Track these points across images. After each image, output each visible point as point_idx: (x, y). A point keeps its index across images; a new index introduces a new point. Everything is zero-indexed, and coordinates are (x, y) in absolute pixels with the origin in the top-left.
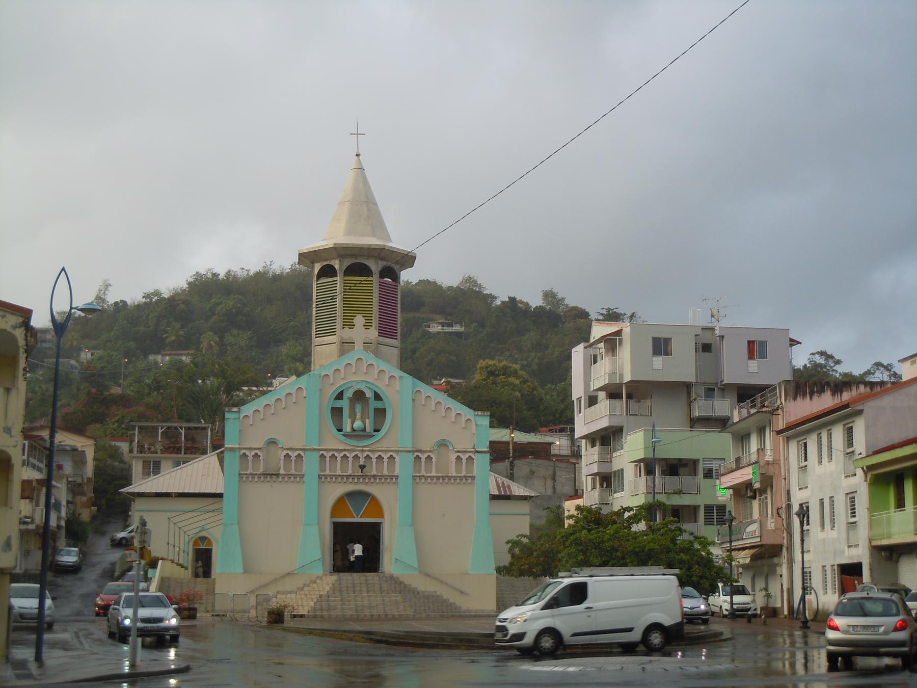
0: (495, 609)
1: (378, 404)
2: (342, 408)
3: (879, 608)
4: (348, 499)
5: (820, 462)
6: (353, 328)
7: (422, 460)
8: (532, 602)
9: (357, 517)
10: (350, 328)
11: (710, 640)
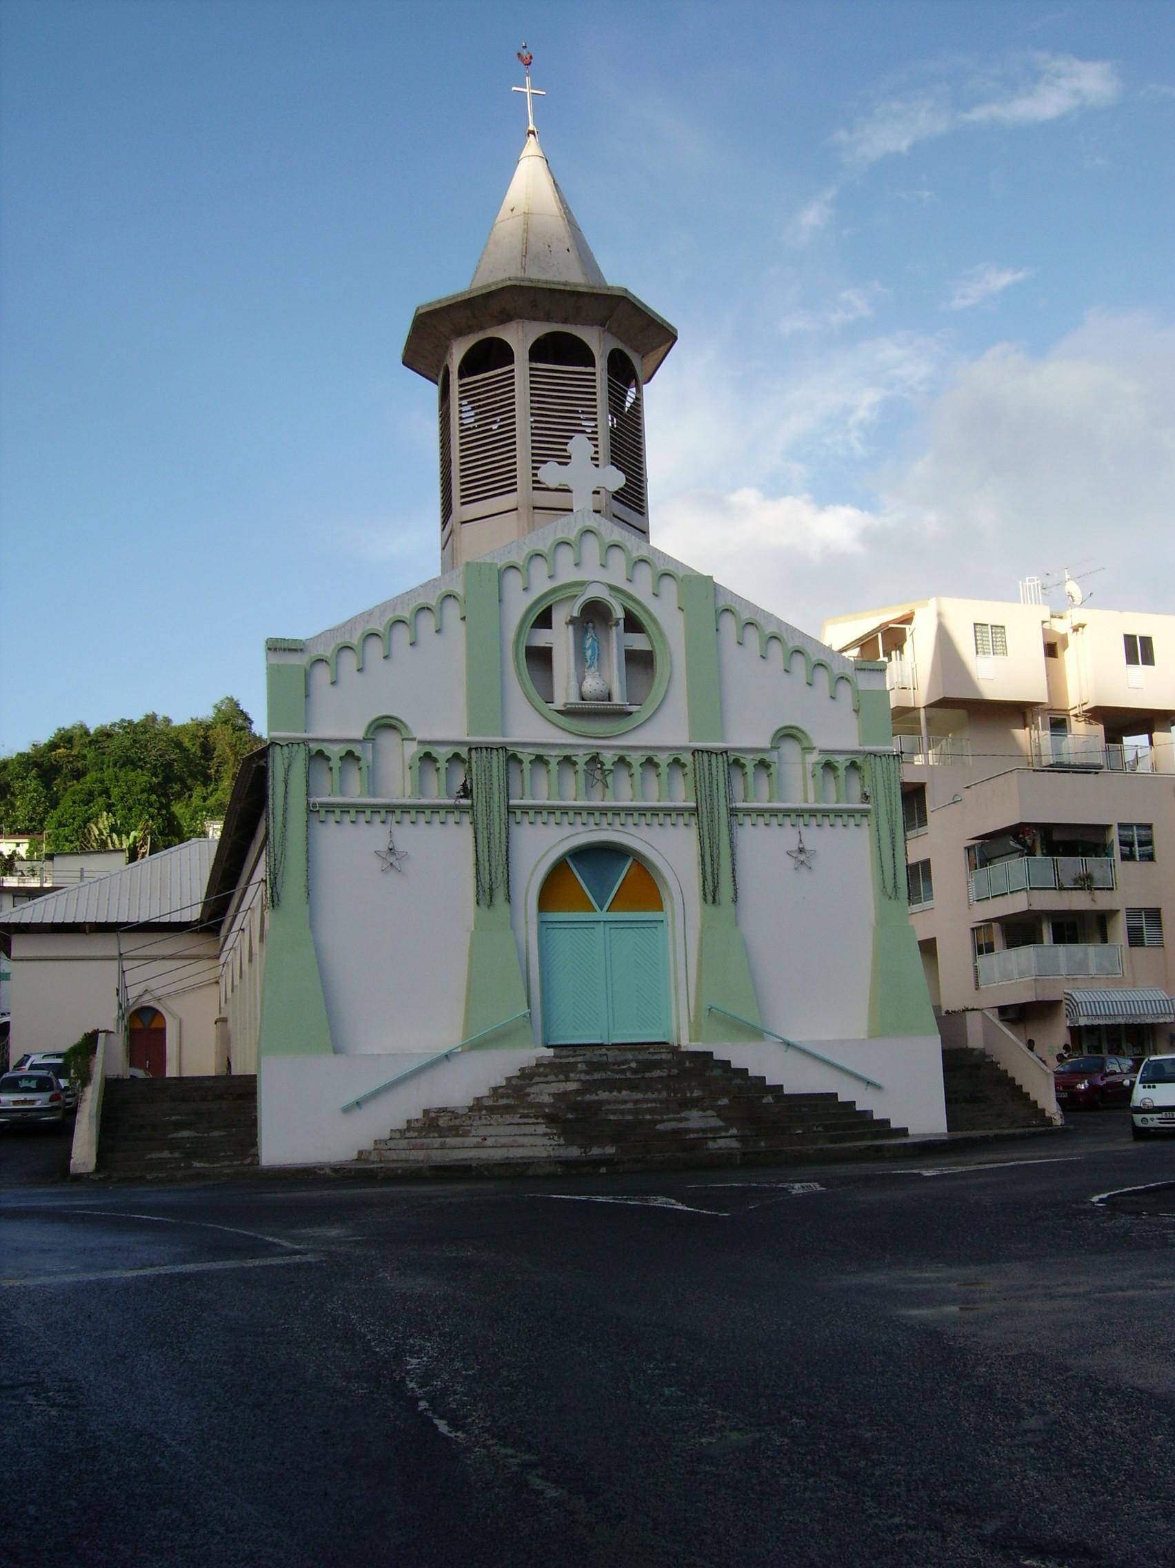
0: (946, 1131)
1: (638, 642)
2: (551, 649)
3: (33, 1084)
4: (575, 865)
5: (1159, 1119)
6: (566, 464)
7: (747, 770)
8: (279, 1249)
9: (601, 910)
10: (560, 463)
11: (654, 1105)
